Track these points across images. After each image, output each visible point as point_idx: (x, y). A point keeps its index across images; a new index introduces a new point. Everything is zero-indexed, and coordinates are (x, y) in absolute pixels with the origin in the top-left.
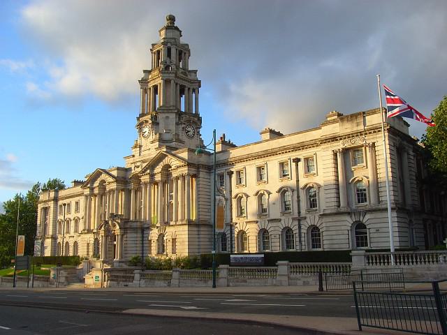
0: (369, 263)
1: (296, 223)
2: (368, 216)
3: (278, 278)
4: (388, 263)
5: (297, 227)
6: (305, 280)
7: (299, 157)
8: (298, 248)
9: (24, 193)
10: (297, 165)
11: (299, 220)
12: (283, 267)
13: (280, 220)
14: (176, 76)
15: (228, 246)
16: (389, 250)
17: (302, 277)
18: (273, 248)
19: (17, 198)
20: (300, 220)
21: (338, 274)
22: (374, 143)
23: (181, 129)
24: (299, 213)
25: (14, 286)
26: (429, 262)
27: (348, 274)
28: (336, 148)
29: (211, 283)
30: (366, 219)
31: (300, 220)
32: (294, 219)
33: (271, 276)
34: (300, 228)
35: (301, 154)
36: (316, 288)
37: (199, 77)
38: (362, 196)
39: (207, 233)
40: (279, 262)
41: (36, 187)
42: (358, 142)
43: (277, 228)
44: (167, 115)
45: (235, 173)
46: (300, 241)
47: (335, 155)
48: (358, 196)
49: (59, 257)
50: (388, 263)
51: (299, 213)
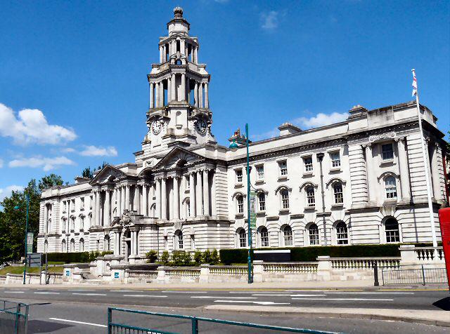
0: (419, 258)
3: (319, 273)
4: (432, 258)
6: (348, 274)
9: (20, 189)
12: (324, 264)
14: (186, 71)
16: (432, 245)
17: (346, 272)
19: (316, 117)
21: (344, 269)
22: (405, 138)
24: (324, 208)
25: (24, 283)
26: (424, 258)
27: (397, 269)
28: (364, 144)
29: (245, 278)
30: (397, 214)
33: (314, 271)
36: (370, 282)
38: (339, 197)
41: (32, 183)
42: (394, 135)
47: (364, 149)
49: (441, 232)
50: (432, 258)
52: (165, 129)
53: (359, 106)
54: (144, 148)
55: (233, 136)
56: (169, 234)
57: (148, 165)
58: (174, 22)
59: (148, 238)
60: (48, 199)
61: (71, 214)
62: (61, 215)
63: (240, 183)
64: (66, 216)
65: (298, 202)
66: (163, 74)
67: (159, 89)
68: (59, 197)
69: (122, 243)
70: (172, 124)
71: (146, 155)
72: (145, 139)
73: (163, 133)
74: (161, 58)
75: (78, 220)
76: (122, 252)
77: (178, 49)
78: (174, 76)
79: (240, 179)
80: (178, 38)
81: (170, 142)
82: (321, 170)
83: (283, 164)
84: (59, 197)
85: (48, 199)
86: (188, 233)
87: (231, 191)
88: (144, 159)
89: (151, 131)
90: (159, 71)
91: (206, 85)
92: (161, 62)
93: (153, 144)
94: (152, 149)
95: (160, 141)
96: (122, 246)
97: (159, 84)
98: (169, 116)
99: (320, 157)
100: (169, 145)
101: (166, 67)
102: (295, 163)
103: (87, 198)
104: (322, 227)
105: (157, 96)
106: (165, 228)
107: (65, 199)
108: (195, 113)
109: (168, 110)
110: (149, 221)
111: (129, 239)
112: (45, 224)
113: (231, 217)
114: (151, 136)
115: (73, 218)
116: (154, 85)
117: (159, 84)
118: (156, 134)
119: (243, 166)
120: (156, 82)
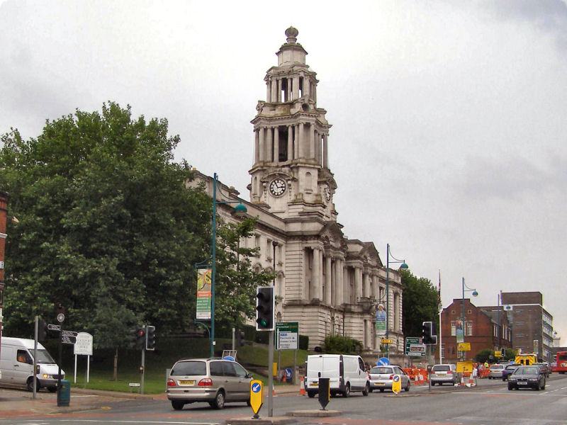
23: (323, 190)
37: (328, 118)
39: (353, 325)
44: (308, 170)
78: (301, 127)
80: (302, 74)
90: (272, 114)
97: (273, 130)
107: (270, 236)
117: (273, 130)
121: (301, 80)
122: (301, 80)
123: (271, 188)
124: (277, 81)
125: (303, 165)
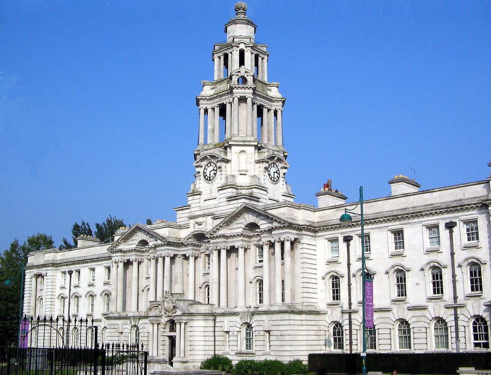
1: (346, 316)
2: (141, 322)
5: (453, 318)
7: (454, 220)
8: (454, 346)
10: (71, 277)
11: (350, 314)
13: (424, 308)
14: (254, 94)
15: (346, 342)
18: (381, 347)
20: (455, 308)
31: (455, 308)
32: (343, 312)
34: (456, 319)
35: (73, 268)
40: (461, 369)
43: (422, 319)
45: (74, 272)
46: (457, 337)
48: (434, 286)
51: (350, 304)
52: (223, 177)
53: (401, 176)
54: (191, 200)
55: (323, 190)
56: (231, 329)
57: (197, 227)
58: (234, 22)
59: (303, 343)
60: (38, 267)
61: (73, 290)
62: (58, 292)
63: (260, 264)
64: (66, 293)
65: (419, 288)
66: (219, 95)
67: (214, 118)
68: (55, 265)
69: (161, 338)
70: (228, 169)
71: (195, 210)
72: (192, 187)
73: (219, 181)
74: (216, 73)
75: (84, 302)
76: (161, 352)
77: (242, 62)
78: (236, 100)
79: (336, 249)
80: (242, 46)
81: (230, 195)
82: (138, 269)
83: (398, 234)
84: (55, 265)
85: (38, 267)
86: (261, 328)
87: (322, 269)
88: (191, 218)
89: (202, 177)
90: (212, 92)
91: (279, 113)
92: (216, 78)
93: (203, 197)
94: (203, 204)
95: (216, 194)
96: (161, 343)
97: (213, 109)
98: (229, 157)
99: (450, 226)
100: (230, 199)
101: (224, 86)
102: (416, 234)
103: (100, 270)
104: (453, 323)
105: (210, 127)
106: (226, 319)
107: (66, 269)
108: (265, 155)
109: (226, 147)
110: (203, 309)
111: (172, 334)
112: (33, 304)
113: (322, 306)
114: (201, 184)
115: (92, 296)
116: (206, 111)
117: (213, 109)
118: (209, 179)
119: (441, 221)
120: (209, 107)
121: (242, 53)
122: (242, 53)
123: (204, 173)
124: (220, 58)
125: (236, 143)
